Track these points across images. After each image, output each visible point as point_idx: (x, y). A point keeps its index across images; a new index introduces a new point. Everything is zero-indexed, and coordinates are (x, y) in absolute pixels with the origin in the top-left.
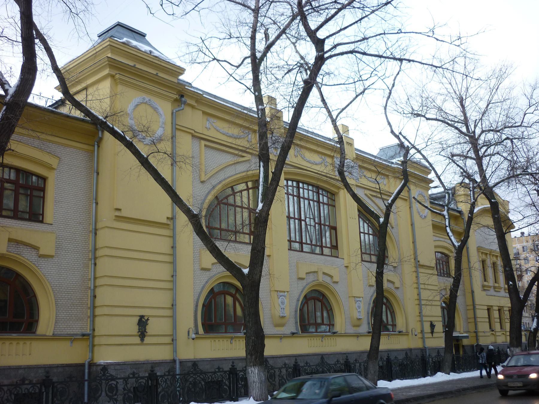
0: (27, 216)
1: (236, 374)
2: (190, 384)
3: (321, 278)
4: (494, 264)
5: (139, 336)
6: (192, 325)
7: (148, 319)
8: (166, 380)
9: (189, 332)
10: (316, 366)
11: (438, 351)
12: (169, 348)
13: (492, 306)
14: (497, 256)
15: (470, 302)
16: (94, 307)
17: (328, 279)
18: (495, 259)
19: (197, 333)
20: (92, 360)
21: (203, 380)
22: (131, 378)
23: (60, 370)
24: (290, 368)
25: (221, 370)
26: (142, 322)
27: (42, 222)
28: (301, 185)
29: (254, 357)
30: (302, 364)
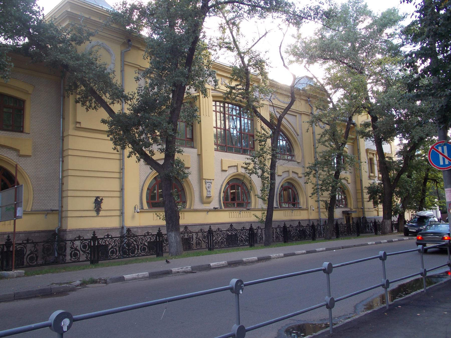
0: (11, 128)
1: (253, 231)
3: (292, 175)
4: (371, 160)
5: (96, 211)
6: (138, 203)
7: (102, 199)
8: (105, 241)
9: (135, 208)
10: (226, 231)
11: (94, 232)
12: (117, 219)
14: (373, 154)
15: (359, 187)
16: (62, 191)
17: (295, 176)
18: (371, 156)
19: (142, 208)
20: (61, 227)
21: (135, 241)
22: (77, 240)
23: (37, 235)
24: (205, 232)
25: (30, 242)
26: (98, 202)
27: (22, 132)
28: (226, 105)
29: (171, 225)
30: (288, 226)
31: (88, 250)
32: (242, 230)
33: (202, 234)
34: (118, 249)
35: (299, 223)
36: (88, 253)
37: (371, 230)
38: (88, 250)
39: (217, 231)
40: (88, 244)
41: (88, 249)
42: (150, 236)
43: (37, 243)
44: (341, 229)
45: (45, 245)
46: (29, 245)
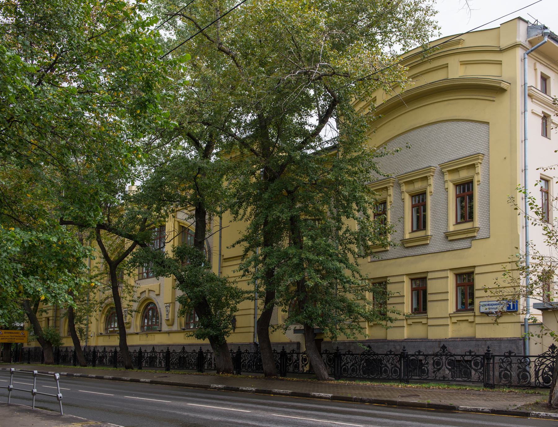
2: (546, 367)
13: (474, 267)
22: (468, 355)
24: (234, 353)
25: (392, 353)
31: (480, 369)
32: (192, 353)
33: (327, 356)
34: (358, 367)
35: (154, 348)
36: (480, 372)
37: (160, 363)
38: (480, 369)
39: (346, 354)
40: (481, 362)
41: (481, 367)
42: (393, 356)
43: (427, 355)
44: (174, 360)
45: (435, 358)
46: (294, 355)
